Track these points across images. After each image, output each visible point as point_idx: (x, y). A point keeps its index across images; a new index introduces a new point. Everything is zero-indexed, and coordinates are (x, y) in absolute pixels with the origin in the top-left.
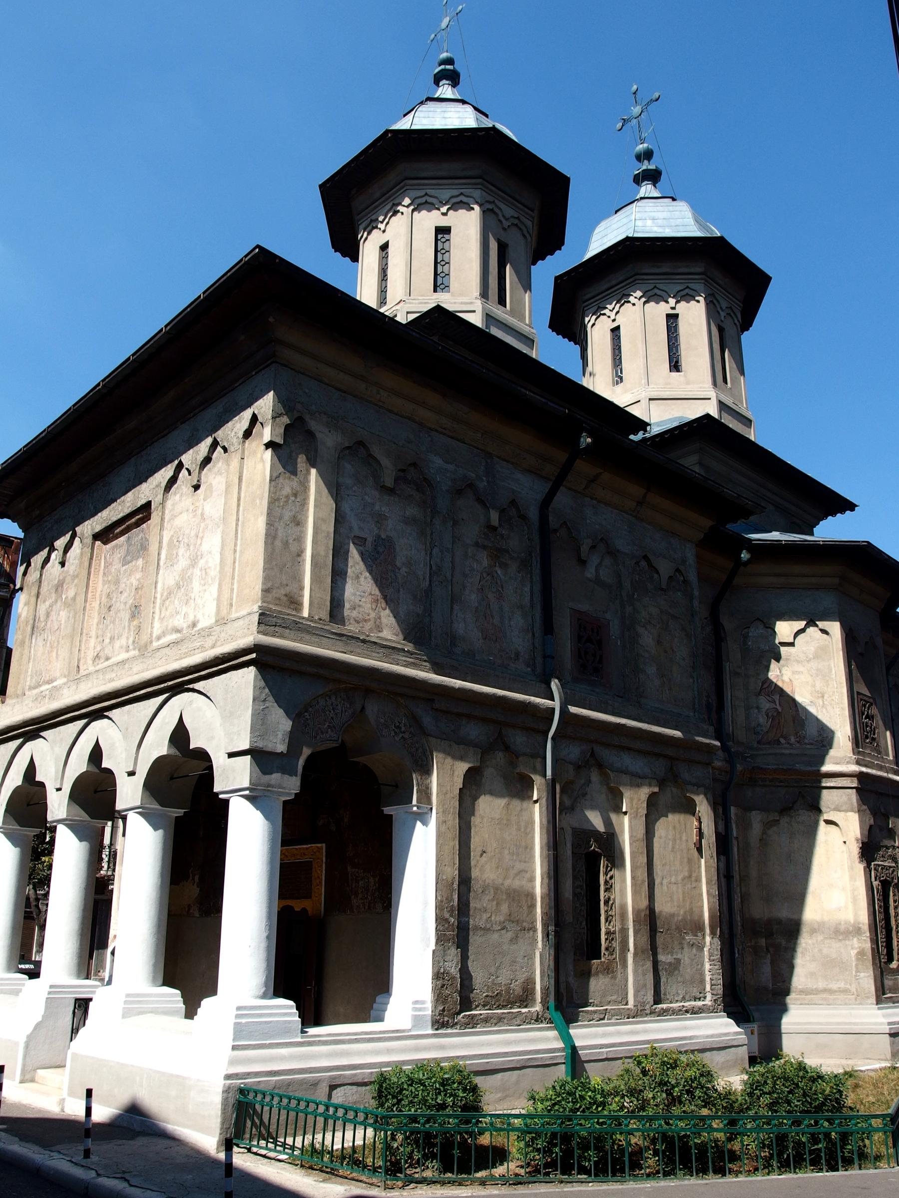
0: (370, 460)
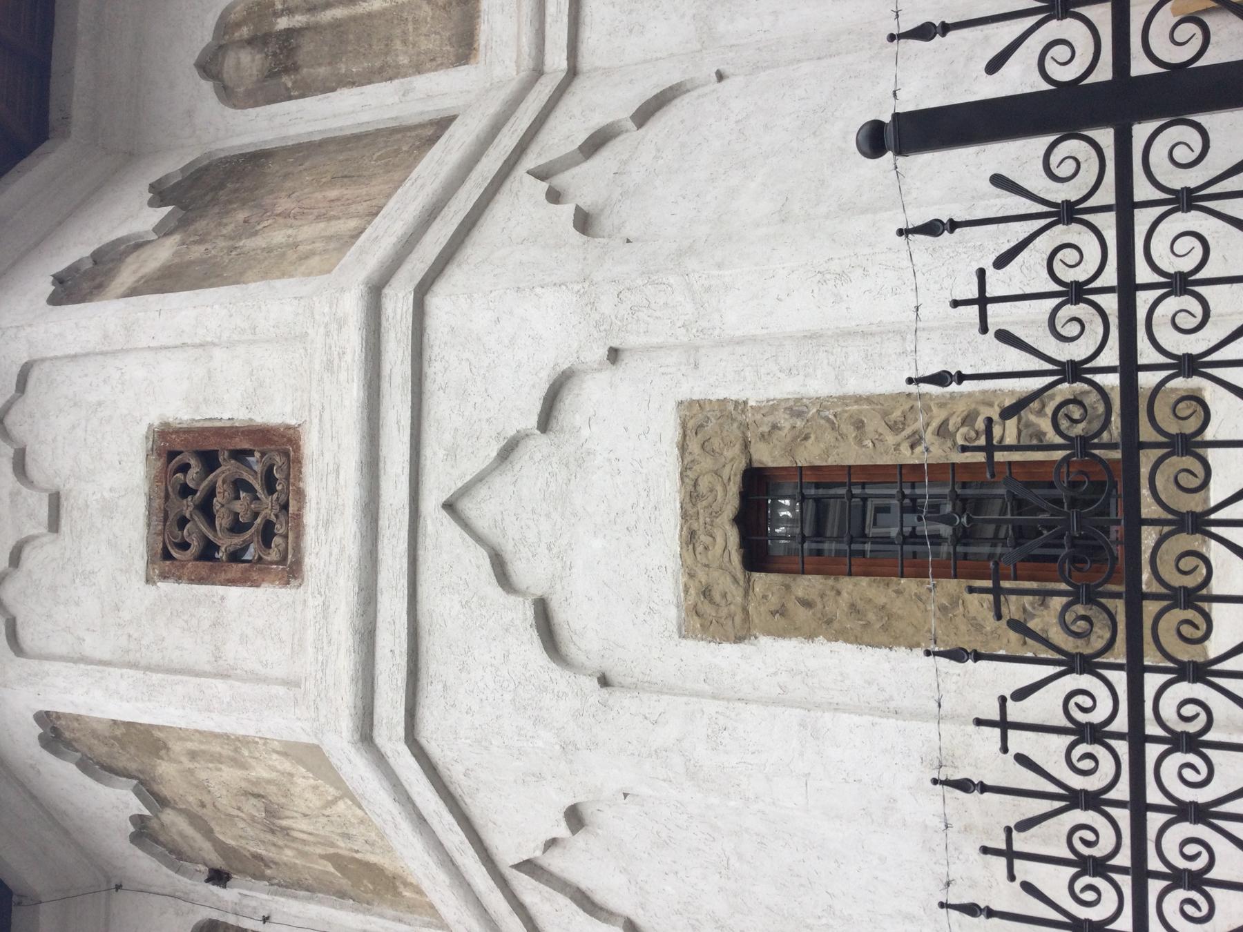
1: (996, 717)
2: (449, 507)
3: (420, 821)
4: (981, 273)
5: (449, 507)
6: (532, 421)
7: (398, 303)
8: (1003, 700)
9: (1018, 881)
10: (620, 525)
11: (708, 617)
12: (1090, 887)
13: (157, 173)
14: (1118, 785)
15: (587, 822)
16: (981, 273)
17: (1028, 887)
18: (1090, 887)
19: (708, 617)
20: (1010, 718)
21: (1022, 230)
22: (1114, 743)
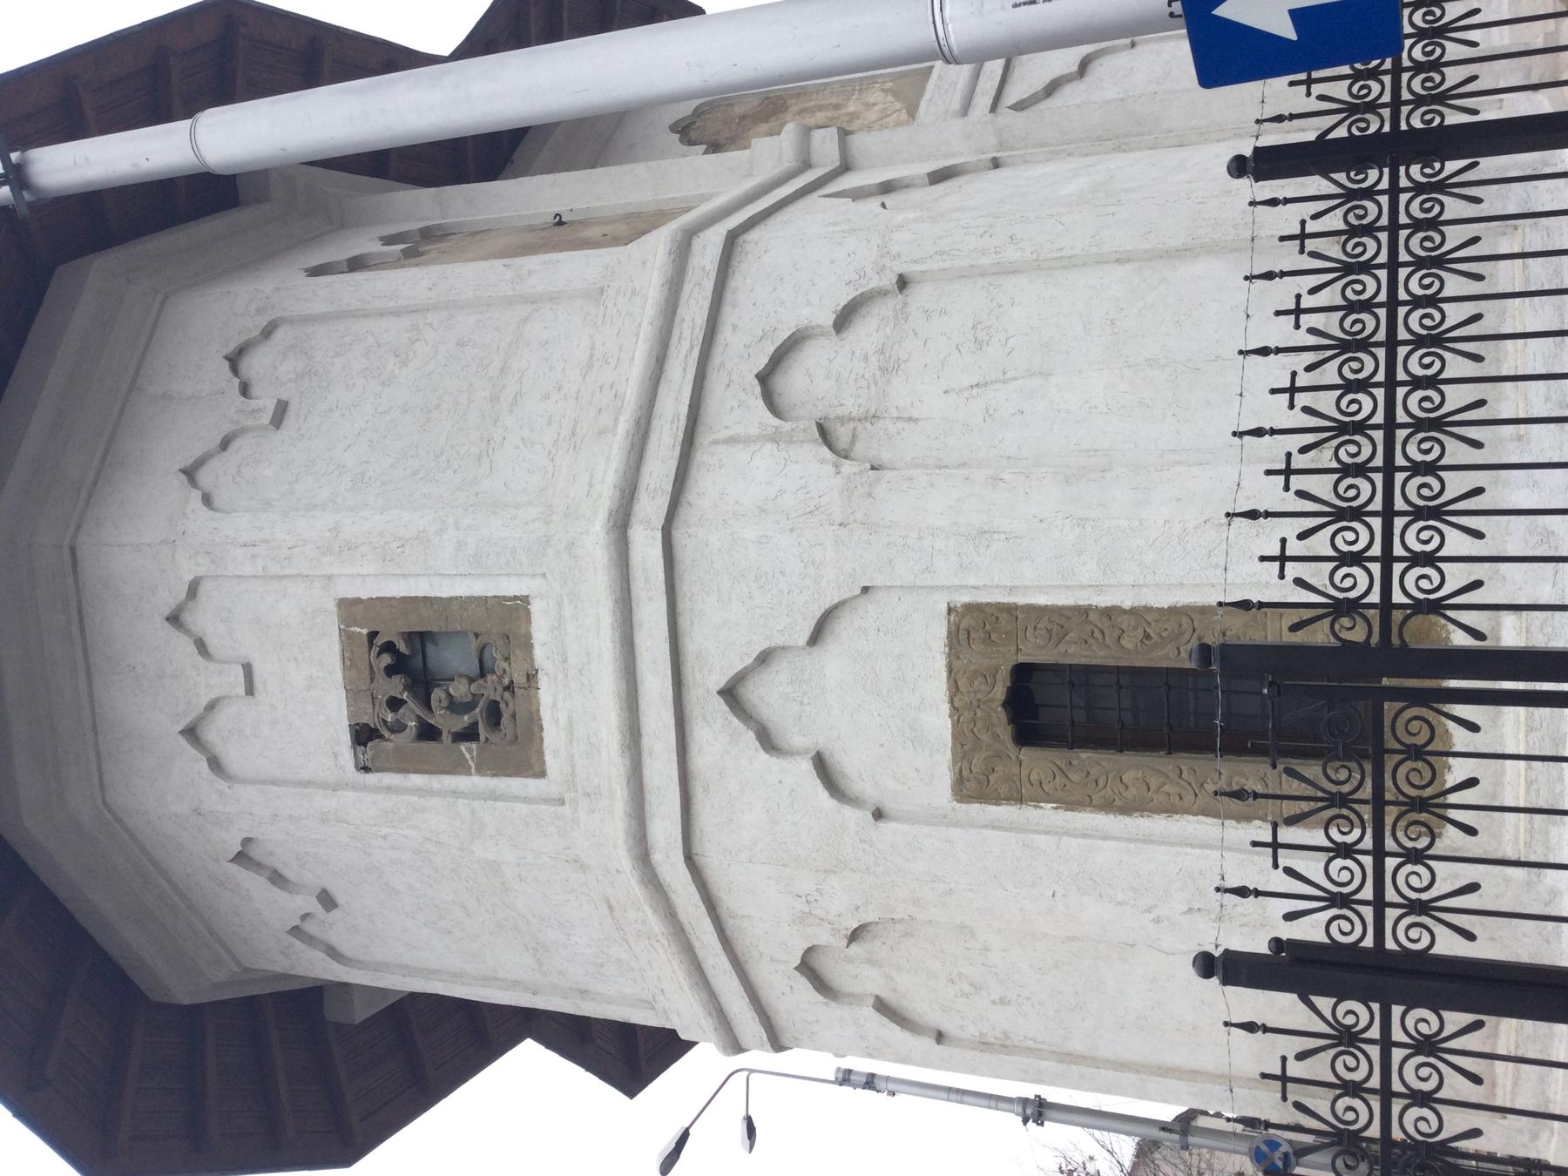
1: (1278, 1072)
2: (731, 694)
3: (670, 914)
4: (1289, 455)
5: (731, 694)
6: (828, 319)
7: (714, 238)
8: (1284, 1059)
9: (1289, 1102)
10: (898, 706)
11: (976, 784)
12: (1350, 487)
13: (481, 725)
14: (1393, 713)
15: (843, 335)
16: (1289, 455)
17: (1290, 872)
18: (1350, 487)
19: (976, 784)
20: (1289, 1073)
21: (1329, 353)
22: (1404, 1090)
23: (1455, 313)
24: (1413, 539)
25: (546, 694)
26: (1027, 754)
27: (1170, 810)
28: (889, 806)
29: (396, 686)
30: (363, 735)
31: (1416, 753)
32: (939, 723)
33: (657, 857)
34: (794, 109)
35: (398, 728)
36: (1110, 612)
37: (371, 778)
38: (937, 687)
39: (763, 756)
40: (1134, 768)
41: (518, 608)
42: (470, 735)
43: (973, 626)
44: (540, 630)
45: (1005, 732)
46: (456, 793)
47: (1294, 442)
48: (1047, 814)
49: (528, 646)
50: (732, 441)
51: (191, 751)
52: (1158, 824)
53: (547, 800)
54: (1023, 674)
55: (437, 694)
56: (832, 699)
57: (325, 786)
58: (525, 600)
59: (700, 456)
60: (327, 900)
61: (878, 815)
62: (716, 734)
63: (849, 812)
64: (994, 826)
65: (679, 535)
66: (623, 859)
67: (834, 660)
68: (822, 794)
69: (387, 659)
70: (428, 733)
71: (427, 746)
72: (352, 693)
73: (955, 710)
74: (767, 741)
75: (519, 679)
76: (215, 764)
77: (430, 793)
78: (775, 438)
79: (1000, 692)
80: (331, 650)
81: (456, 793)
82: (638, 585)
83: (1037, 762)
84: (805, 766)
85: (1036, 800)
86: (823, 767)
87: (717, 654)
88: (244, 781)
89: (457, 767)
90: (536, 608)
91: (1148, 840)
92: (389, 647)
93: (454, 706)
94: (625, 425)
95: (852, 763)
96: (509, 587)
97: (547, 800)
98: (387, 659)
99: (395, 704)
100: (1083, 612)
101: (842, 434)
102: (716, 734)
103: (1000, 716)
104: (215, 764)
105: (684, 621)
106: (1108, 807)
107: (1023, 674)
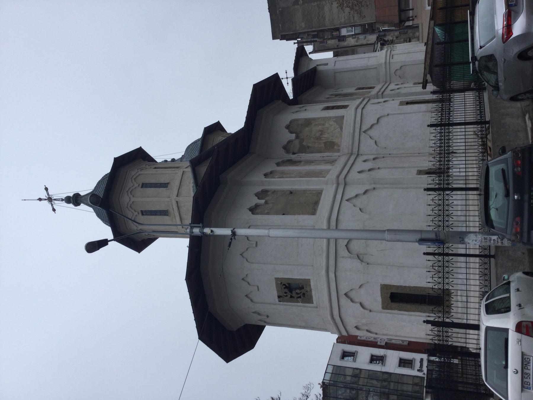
0: (290, 142)
5: (346, 294)
10: (374, 298)
11: (385, 307)
19: (385, 307)
23: (451, 280)
24: (446, 219)
25: (313, 293)
26: (393, 304)
27: (414, 311)
28: (372, 310)
29: (286, 290)
30: (279, 297)
31: (448, 301)
32: (379, 299)
33: (334, 317)
34: (313, 124)
35: (287, 296)
36: (405, 287)
37: (281, 303)
38: (379, 294)
39: (352, 303)
40: (408, 306)
41: (309, 281)
42: (300, 297)
43: (384, 287)
44: (312, 284)
45: (390, 301)
46: (298, 306)
47: (433, 217)
48: (396, 311)
49: (310, 286)
50: (343, 257)
51: (247, 299)
52: (412, 313)
53: (314, 307)
54: (392, 294)
55: (294, 292)
56: (362, 296)
57: (273, 304)
58: (309, 279)
59: (338, 260)
60: (268, 316)
61: (370, 311)
62: (344, 301)
63: (366, 311)
64: (388, 313)
65: (337, 274)
66: (329, 318)
67: (362, 291)
68: (361, 309)
69: (284, 286)
70: (291, 297)
71: (291, 299)
72: (278, 291)
73: (382, 298)
74: (352, 301)
75: (308, 290)
76: (251, 300)
77: (293, 306)
78: (350, 257)
79: (389, 296)
80: (274, 285)
81: (298, 306)
82: (330, 280)
83: (394, 305)
84: (359, 305)
85: (394, 310)
86: (361, 305)
87: (344, 288)
88: (257, 303)
89: (298, 302)
90: (311, 281)
91: (411, 315)
92: (284, 285)
93: (297, 294)
94: (325, 254)
95: (366, 304)
96: (307, 278)
97: (314, 307)
98: (284, 286)
99: (286, 293)
100: (401, 286)
101: (361, 257)
102: (344, 301)
103: (389, 299)
104: (251, 300)
105: (338, 284)
106: (405, 311)
107: (392, 294)
